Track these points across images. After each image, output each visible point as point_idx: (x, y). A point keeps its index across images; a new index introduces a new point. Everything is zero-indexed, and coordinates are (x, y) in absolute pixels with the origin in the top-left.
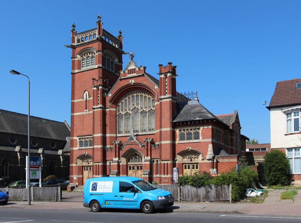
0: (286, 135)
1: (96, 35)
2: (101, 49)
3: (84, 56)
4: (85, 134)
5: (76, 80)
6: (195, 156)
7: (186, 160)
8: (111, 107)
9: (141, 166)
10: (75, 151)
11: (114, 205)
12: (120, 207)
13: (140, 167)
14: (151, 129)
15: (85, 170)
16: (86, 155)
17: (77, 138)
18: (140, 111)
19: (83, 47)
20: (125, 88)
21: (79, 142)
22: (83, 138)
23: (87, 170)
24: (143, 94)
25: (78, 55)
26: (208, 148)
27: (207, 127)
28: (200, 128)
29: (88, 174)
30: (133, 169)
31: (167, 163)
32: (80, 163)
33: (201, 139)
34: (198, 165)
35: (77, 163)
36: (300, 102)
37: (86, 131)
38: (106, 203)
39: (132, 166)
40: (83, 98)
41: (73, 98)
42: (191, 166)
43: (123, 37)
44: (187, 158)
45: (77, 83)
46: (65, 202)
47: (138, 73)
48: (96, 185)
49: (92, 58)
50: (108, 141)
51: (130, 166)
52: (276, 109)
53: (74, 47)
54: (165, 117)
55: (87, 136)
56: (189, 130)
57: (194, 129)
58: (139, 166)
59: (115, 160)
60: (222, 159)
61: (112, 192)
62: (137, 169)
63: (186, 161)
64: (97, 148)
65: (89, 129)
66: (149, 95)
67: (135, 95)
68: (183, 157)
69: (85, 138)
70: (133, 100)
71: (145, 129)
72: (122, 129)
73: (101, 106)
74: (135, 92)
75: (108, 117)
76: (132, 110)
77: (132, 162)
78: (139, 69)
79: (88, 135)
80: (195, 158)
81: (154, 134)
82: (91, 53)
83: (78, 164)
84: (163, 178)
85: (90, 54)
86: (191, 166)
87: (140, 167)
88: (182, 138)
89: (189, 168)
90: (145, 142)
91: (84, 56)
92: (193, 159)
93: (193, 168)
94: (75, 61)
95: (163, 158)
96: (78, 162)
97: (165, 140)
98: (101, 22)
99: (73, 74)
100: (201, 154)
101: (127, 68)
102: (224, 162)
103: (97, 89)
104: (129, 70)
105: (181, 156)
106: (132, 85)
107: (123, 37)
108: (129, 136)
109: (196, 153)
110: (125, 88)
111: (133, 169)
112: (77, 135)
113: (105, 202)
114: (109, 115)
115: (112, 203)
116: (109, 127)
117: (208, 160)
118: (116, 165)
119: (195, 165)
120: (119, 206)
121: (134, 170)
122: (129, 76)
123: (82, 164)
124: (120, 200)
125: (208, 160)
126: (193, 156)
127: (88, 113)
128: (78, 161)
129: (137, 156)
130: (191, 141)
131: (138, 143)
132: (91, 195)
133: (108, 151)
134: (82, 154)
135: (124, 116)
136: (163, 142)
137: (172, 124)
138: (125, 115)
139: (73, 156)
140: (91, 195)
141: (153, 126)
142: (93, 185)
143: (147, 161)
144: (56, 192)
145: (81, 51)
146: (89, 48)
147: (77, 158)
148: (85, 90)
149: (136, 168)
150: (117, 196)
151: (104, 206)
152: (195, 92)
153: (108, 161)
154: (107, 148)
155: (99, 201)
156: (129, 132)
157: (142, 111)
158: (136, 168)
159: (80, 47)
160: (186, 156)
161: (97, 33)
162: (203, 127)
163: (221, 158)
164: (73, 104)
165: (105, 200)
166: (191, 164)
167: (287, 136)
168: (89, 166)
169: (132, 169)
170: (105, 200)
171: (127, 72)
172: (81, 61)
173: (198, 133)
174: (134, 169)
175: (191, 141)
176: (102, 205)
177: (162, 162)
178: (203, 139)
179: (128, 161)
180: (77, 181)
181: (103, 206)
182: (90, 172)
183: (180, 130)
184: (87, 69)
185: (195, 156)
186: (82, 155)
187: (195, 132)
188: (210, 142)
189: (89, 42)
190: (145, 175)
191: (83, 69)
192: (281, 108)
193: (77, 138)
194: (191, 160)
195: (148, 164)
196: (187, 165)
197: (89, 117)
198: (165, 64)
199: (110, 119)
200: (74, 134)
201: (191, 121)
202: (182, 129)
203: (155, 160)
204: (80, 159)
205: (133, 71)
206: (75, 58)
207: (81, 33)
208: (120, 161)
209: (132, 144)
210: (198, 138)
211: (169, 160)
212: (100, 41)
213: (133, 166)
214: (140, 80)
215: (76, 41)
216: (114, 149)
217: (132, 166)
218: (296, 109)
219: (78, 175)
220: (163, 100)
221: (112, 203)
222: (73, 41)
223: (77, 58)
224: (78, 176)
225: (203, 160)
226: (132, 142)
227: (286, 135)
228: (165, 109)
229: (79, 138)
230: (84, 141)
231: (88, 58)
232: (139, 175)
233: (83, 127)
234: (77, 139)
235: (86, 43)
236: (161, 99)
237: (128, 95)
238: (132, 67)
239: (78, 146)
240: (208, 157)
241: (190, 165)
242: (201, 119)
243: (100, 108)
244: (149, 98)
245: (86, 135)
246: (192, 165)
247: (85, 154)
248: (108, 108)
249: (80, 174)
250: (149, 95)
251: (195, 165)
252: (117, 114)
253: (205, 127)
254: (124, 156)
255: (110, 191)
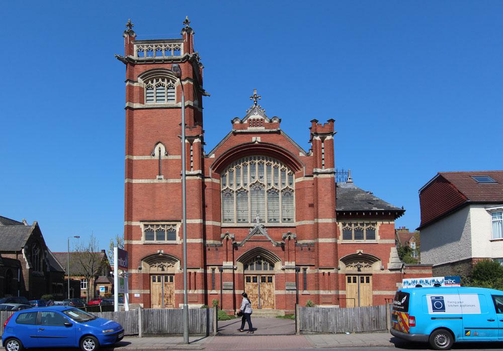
0: (491, 241)
1: (179, 50)
2: (191, 77)
3: (150, 82)
4: (158, 219)
5: (135, 121)
6: (169, 264)
7: (352, 269)
8: (213, 176)
9: (268, 277)
10: (137, 246)
11: (485, 336)
12: (499, 339)
13: (267, 278)
14: (287, 220)
15: (362, 282)
16: (161, 255)
17: (142, 225)
18: (266, 189)
19: (151, 65)
20: (237, 150)
21: (145, 231)
22: (152, 225)
23: (159, 281)
24: (272, 162)
25: (139, 78)
26: (391, 253)
27: (388, 223)
28: (376, 223)
29: (162, 288)
30: (253, 282)
31: (329, 273)
32: (146, 268)
33: (378, 239)
34: (174, 277)
35: (140, 269)
36: (501, 200)
37: (160, 213)
38: (469, 332)
39: (252, 276)
40: (154, 155)
41: (130, 151)
42: (358, 278)
43: (203, 68)
44: (156, 266)
45: (137, 127)
46: (250, 337)
47: (266, 126)
48: (443, 302)
49: (168, 89)
50: (209, 232)
51: (247, 276)
52: (478, 206)
53: (130, 63)
54: (323, 201)
55: (162, 221)
56: (359, 225)
57: (367, 224)
58: (265, 277)
59: (226, 265)
60: (410, 269)
61: (480, 313)
62: (262, 282)
63: (154, 270)
64: (325, 244)
65: (168, 211)
66: (281, 165)
67: (257, 161)
68: (150, 265)
69: (158, 225)
70: (253, 170)
71: (245, 218)
72: (226, 215)
73: (200, 172)
74: (249, 158)
75: (208, 192)
76: (251, 186)
77: (252, 269)
78: (271, 121)
79: (167, 219)
80: (168, 267)
81: (295, 227)
82: (166, 80)
83: (143, 271)
84: (323, 295)
85: (163, 80)
86: (358, 278)
87: (267, 278)
88: (347, 236)
89: (355, 281)
90: (285, 238)
91: (150, 82)
92: (165, 268)
93: (362, 282)
94: (133, 87)
95: (321, 264)
96: (142, 266)
97: (324, 236)
98: (192, 32)
99: (130, 109)
100: (179, 261)
101: (247, 116)
102: (412, 274)
103: (188, 142)
104: (250, 120)
105: (345, 263)
106: (257, 146)
107: (203, 68)
108: (252, 227)
109: (369, 259)
110: (237, 150)
111: (253, 282)
112: (141, 218)
113: (467, 332)
114: (211, 190)
115: (482, 333)
116: (211, 210)
117: (391, 270)
118: (230, 273)
119: (365, 277)
120: (497, 338)
121: (255, 283)
122: (250, 129)
123: (149, 270)
124: (500, 327)
125: (391, 270)
126: (166, 264)
127: (164, 181)
128: (142, 264)
129: (262, 261)
130: (362, 241)
131: (270, 239)
132: (433, 318)
133: (209, 250)
134: (153, 254)
135: (235, 194)
136: (321, 240)
137: (337, 214)
138: (236, 192)
139: (131, 255)
140: (433, 318)
141: (293, 214)
142: (433, 302)
143: (291, 269)
144: (205, 317)
145: (146, 72)
146: (164, 69)
147: (142, 260)
148: (158, 141)
149: (259, 279)
150: (494, 320)
151: (461, 338)
152: (346, 170)
153: (210, 267)
154: (208, 245)
155: (454, 332)
156: (244, 220)
157: (270, 190)
158: (259, 279)
159: (144, 65)
160: (156, 264)
161: (182, 47)
162: (381, 222)
163: (408, 268)
164: (130, 163)
165: (465, 328)
166: (358, 275)
167: (493, 242)
168: (163, 274)
169: (252, 281)
170: (465, 328)
171: (246, 122)
172: (145, 89)
173: (373, 231)
174: (257, 282)
175: (362, 241)
176: (458, 337)
177: (320, 270)
178: (381, 239)
179: (245, 267)
180: (142, 300)
181: (460, 338)
182: (166, 285)
183: (344, 225)
184: (157, 105)
185: (169, 264)
186: (154, 255)
187: (368, 228)
188: (392, 244)
189: (166, 60)
190: (291, 291)
191: (149, 104)
192: (484, 206)
193: (142, 225)
194: (359, 270)
195: (292, 273)
196: (352, 277)
197: (166, 189)
198: (322, 121)
199: (212, 195)
200: (133, 216)
201: (367, 212)
202: (347, 222)
203: (302, 267)
204: (147, 261)
205: (255, 123)
206: (134, 82)
207: (148, 42)
208: (235, 268)
209: (259, 241)
210: (373, 238)
211: (333, 269)
212: (190, 62)
213: (255, 276)
214: (272, 140)
215: (135, 53)
216: (224, 247)
217: (252, 276)
218: (498, 209)
219: (144, 289)
220: (320, 176)
221: (482, 333)
222: (131, 53)
223: (137, 82)
224: (143, 292)
225: (382, 269)
226: (258, 238)
227: (491, 241)
228: (323, 189)
229: (144, 225)
230: (156, 231)
231: (159, 88)
232: (266, 291)
233: (155, 206)
234: (139, 226)
235: (161, 60)
236: (317, 173)
237: (242, 160)
238: (256, 116)
239: (143, 238)
240: (390, 266)
241: (357, 276)
242: (383, 209)
243: (197, 175)
244: (276, 168)
245: (161, 219)
246: (360, 277)
247: (159, 253)
248: (209, 178)
249: (147, 289)
250: (281, 165)
251: (365, 277)
252: (222, 190)
253: (384, 223)
254: (241, 260)
255: (477, 310)
